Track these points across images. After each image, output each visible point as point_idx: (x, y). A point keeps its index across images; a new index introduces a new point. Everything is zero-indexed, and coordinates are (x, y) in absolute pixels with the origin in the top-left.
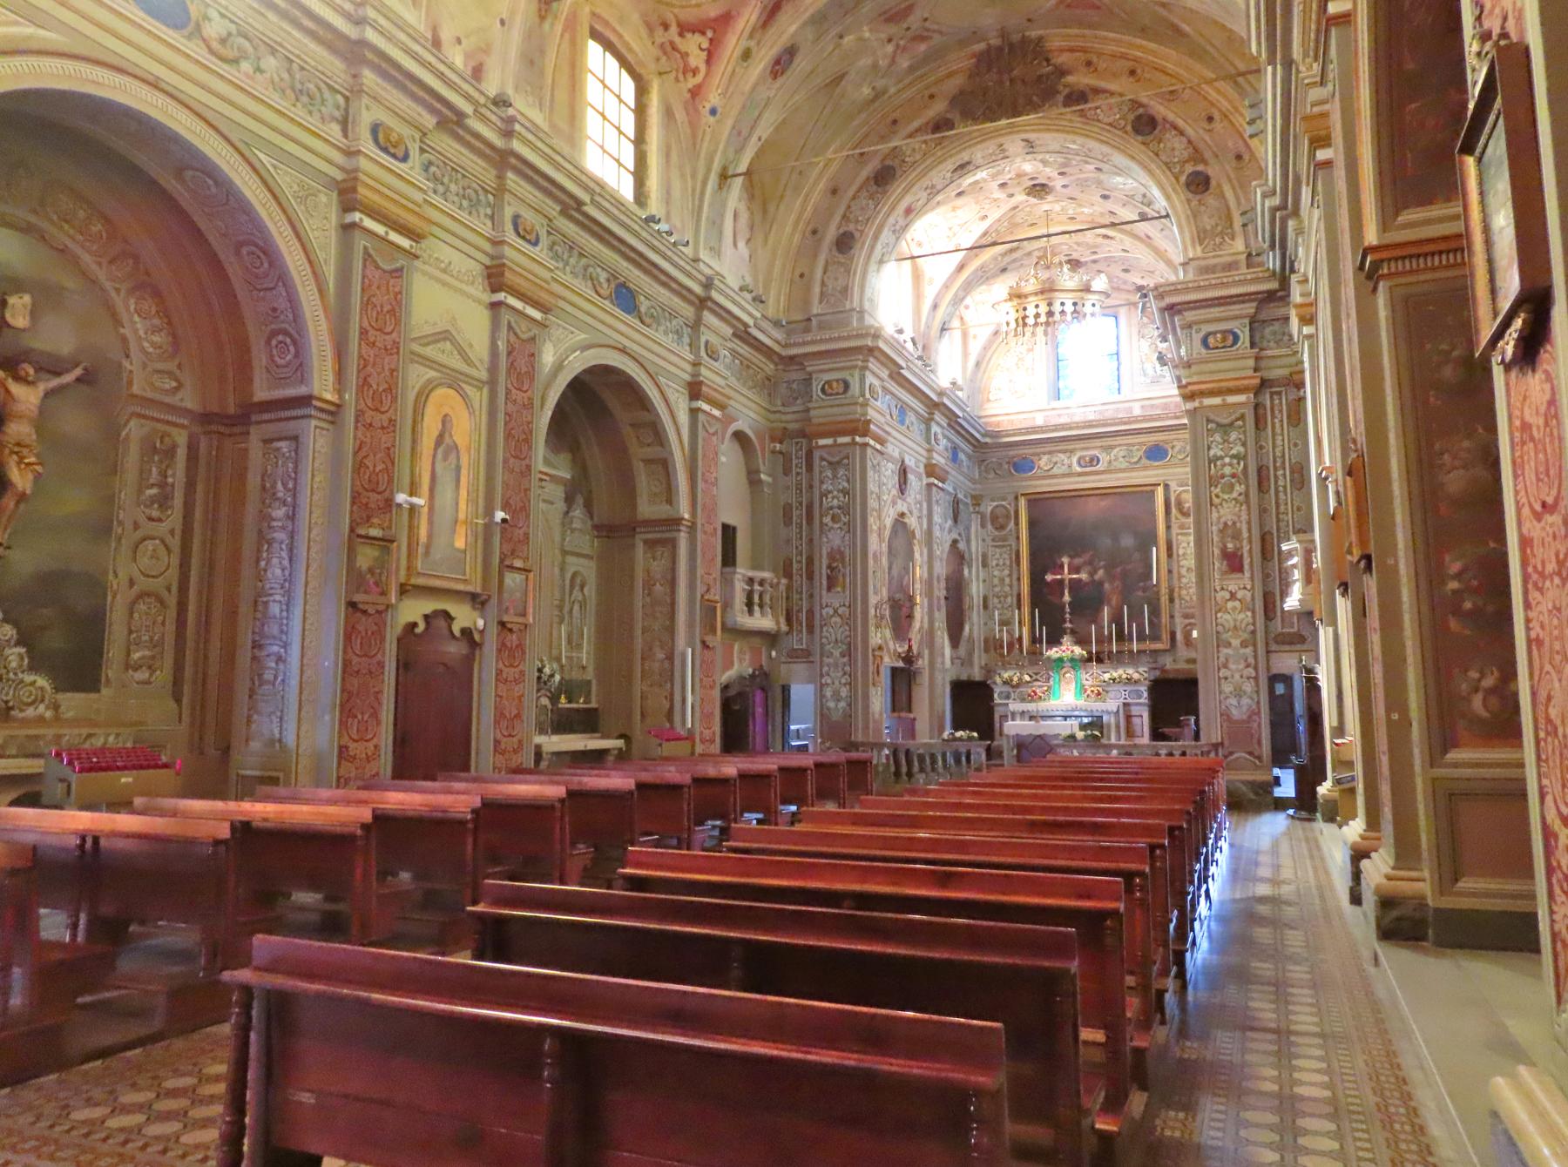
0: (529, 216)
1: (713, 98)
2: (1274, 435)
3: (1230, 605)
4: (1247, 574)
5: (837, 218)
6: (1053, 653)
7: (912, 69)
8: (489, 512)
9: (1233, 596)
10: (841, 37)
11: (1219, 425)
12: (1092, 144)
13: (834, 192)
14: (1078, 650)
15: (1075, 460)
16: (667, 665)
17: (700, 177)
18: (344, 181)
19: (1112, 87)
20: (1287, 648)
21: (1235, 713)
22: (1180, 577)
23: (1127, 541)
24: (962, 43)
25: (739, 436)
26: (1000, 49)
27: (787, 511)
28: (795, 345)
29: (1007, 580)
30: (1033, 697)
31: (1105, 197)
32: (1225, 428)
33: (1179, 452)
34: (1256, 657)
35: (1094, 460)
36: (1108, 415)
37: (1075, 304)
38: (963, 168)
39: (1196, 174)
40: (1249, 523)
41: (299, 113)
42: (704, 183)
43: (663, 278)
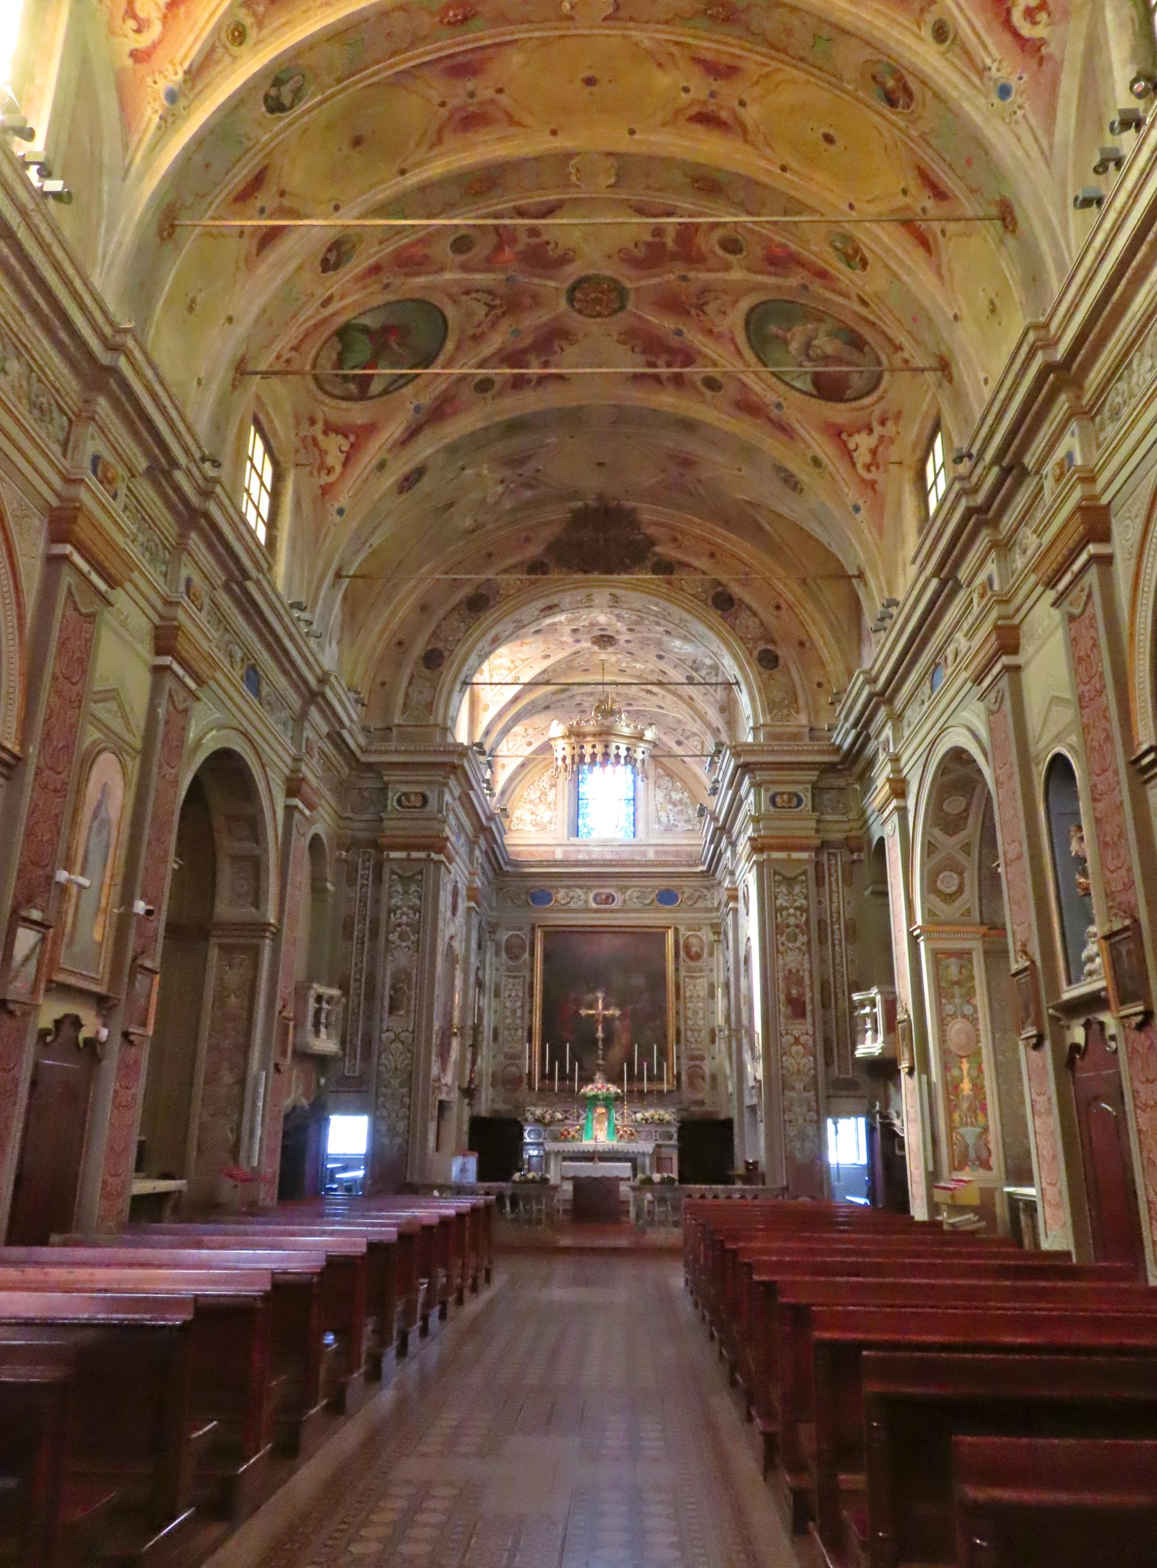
0: (197, 580)
1: (343, 499)
2: (831, 891)
3: (794, 1049)
4: (809, 1020)
5: (426, 635)
6: (588, 1090)
7: (513, 511)
8: (127, 900)
9: (797, 1041)
10: (463, 469)
11: (785, 878)
12: (673, 609)
13: (424, 608)
14: (613, 1089)
15: (591, 896)
16: (236, 1090)
17: (318, 572)
18: (59, 508)
19: (696, 563)
20: (845, 1093)
21: (798, 1155)
22: (686, 1018)
23: (639, 981)
24: (563, 498)
25: (316, 839)
26: (597, 510)
27: (348, 927)
28: (376, 752)
29: (519, 1013)
30: (564, 1137)
31: (660, 657)
32: (790, 881)
33: (689, 898)
34: (817, 1101)
35: (609, 899)
36: (624, 856)
37: (628, 749)
38: (550, 609)
39: (766, 651)
40: (811, 972)
41: (30, 422)
42: (322, 578)
43: (288, 666)
